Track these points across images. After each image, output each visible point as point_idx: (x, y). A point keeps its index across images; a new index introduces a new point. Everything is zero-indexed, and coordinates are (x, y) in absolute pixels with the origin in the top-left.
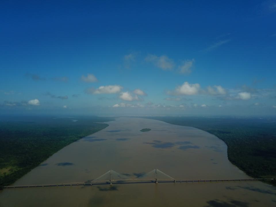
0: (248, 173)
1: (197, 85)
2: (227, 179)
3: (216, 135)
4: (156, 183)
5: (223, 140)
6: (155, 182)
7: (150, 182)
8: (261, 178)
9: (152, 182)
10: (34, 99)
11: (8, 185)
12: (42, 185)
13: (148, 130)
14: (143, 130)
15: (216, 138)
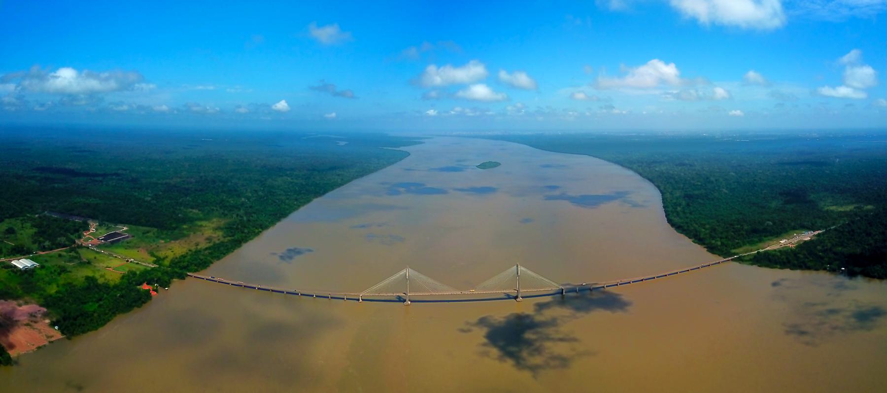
0: (712, 249)
2: (676, 271)
3: (636, 171)
4: (518, 300)
6: (516, 298)
7: (503, 296)
8: (735, 254)
9: (509, 297)
11: (196, 271)
12: (254, 286)
13: (496, 164)
14: (483, 166)
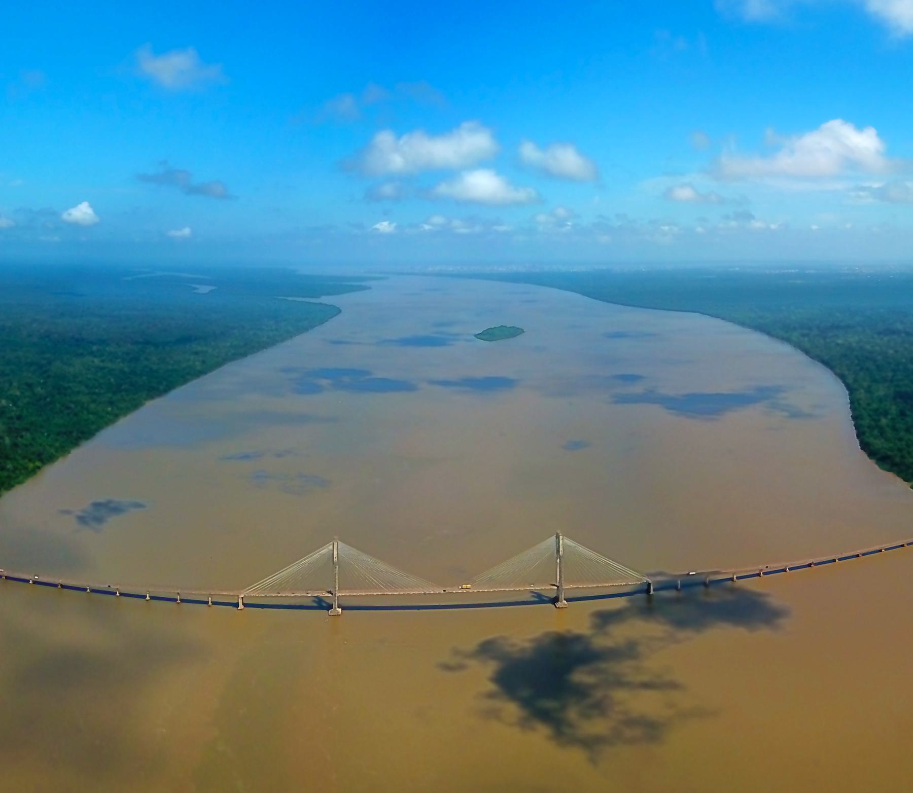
1: (65, 216)
4: (559, 604)
5: (827, 363)
6: (555, 600)
7: (528, 597)
9: (540, 599)
10: (75, 205)
13: (515, 332)
14: (488, 335)
15: (802, 357)
